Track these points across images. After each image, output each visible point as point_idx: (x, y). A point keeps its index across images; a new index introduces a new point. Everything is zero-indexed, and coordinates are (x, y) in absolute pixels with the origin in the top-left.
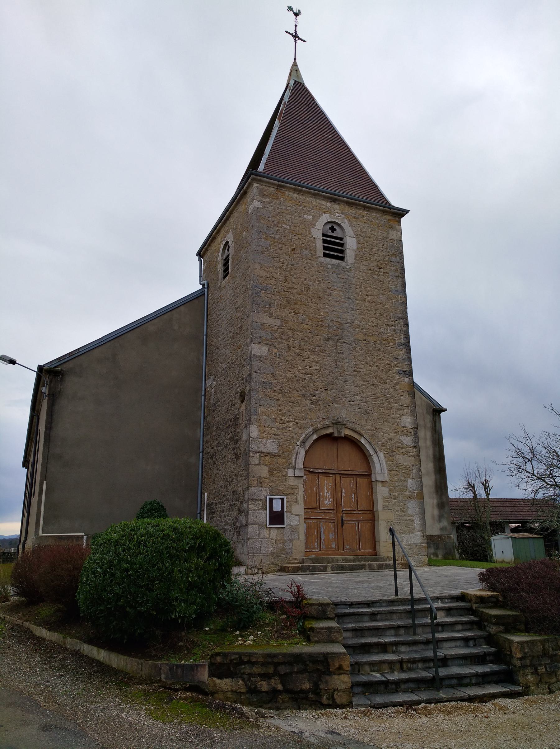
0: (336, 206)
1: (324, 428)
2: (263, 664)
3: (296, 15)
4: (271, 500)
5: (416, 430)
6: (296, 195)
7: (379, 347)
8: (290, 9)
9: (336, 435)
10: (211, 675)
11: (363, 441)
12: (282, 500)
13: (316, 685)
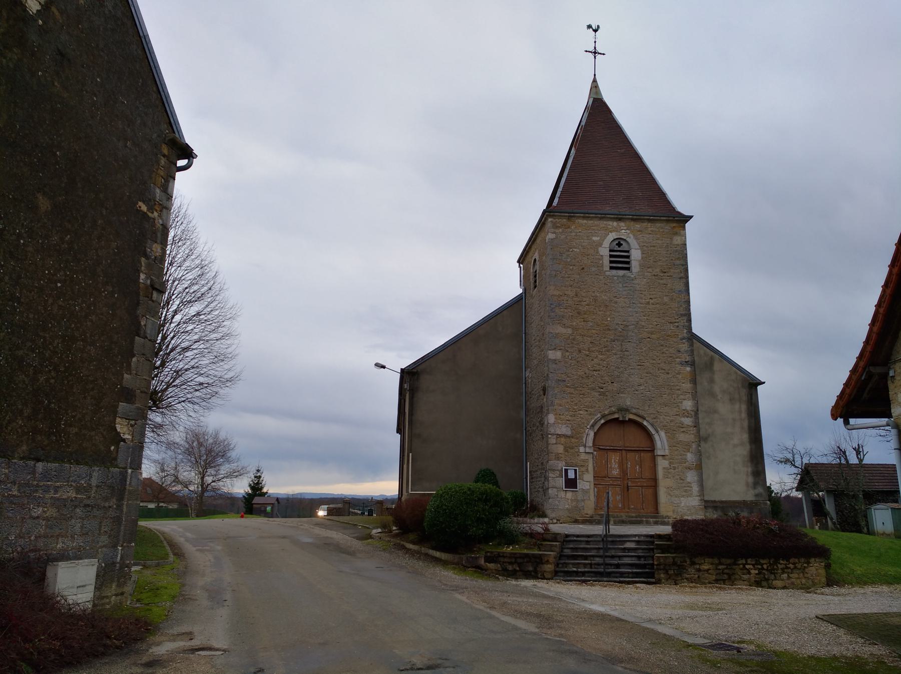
0: (622, 224)
1: (610, 414)
2: (510, 557)
3: (595, 31)
4: (566, 471)
5: (696, 412)
6: (585, 221)
7: (663, 343)
8: (589, 27)
9: (621, 419)
10: (485, 561)
11: (645, 423)
12: (575, 470)
13: (535, 569)
